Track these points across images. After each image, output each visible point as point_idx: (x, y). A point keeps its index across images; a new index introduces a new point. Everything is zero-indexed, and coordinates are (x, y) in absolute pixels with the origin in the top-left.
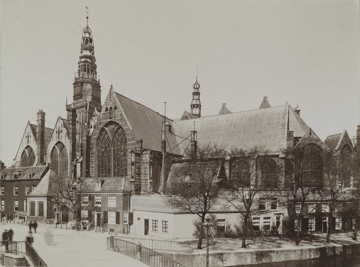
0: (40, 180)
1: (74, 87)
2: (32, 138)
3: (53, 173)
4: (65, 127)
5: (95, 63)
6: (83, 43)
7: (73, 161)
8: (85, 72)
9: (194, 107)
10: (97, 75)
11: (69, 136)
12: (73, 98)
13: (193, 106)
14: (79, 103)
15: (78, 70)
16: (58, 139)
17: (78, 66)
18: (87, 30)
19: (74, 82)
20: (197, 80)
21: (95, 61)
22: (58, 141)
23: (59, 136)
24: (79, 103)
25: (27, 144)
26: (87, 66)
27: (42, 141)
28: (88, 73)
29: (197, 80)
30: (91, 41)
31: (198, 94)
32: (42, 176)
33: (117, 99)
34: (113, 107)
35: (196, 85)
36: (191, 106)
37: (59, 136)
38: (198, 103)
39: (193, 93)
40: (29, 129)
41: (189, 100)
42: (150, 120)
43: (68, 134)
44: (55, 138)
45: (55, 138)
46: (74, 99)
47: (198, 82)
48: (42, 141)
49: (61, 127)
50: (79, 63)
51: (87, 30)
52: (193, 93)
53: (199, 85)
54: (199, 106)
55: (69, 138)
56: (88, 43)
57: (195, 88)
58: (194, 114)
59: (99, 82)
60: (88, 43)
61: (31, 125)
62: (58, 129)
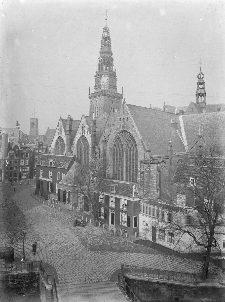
0: (69, 169)
1: (95, 79)
2: (63, 131)
3: (78, 164)
4: (87, 124)
5: (112, 56)
6: (103, 41)
7: (93, 154)
8: (104, 65)
9: (199, 95)
10: (114, 67)
11: (90, 132)
12: (94, 88)
13: (198, 95)
14: (99, 92)
15: (98, 64)
16: (82, 133)
17: (98, 61)
18: (106, 30)
19: (95, 74)
20: (201, 70)
21: (112, 54)
22: (82, 135)
23: (83, 131)
24: (99, 92)
25: (59, 135)
26: (106, 60)
27: (71, 134)
28: (107, 65)
29: (201, 70)
30: (109, 38)
31: (203, 83)
32: (70, 166)
33: (129, 112)
34: (126, 117)
35: (200, 74)
36: (196, 95)
37: (83, 131)
38: (203, 92)
39: (198, 83)
40: (61, 123)
41: (194, 88)
42: (168, 185)
43: (89, 130)
44: (80, 132)
45: (80, 132)
46: (95, 89)
47: (202, 73)
48: (71, 134)
49: (84, 124)
50: (99, 59)
51: (106, 30)
52: (198, 83)
53: (203, 75)
54: (204, 95)
55: (90, 134)
56: (106, 39)
57: (199, 78)
58: (200, 102)
59: (115, 73)
60: (106, 39)
61: (63, 120)
62: (82, 124)
